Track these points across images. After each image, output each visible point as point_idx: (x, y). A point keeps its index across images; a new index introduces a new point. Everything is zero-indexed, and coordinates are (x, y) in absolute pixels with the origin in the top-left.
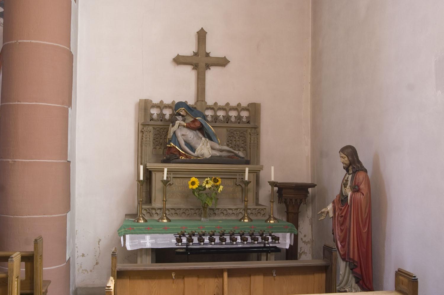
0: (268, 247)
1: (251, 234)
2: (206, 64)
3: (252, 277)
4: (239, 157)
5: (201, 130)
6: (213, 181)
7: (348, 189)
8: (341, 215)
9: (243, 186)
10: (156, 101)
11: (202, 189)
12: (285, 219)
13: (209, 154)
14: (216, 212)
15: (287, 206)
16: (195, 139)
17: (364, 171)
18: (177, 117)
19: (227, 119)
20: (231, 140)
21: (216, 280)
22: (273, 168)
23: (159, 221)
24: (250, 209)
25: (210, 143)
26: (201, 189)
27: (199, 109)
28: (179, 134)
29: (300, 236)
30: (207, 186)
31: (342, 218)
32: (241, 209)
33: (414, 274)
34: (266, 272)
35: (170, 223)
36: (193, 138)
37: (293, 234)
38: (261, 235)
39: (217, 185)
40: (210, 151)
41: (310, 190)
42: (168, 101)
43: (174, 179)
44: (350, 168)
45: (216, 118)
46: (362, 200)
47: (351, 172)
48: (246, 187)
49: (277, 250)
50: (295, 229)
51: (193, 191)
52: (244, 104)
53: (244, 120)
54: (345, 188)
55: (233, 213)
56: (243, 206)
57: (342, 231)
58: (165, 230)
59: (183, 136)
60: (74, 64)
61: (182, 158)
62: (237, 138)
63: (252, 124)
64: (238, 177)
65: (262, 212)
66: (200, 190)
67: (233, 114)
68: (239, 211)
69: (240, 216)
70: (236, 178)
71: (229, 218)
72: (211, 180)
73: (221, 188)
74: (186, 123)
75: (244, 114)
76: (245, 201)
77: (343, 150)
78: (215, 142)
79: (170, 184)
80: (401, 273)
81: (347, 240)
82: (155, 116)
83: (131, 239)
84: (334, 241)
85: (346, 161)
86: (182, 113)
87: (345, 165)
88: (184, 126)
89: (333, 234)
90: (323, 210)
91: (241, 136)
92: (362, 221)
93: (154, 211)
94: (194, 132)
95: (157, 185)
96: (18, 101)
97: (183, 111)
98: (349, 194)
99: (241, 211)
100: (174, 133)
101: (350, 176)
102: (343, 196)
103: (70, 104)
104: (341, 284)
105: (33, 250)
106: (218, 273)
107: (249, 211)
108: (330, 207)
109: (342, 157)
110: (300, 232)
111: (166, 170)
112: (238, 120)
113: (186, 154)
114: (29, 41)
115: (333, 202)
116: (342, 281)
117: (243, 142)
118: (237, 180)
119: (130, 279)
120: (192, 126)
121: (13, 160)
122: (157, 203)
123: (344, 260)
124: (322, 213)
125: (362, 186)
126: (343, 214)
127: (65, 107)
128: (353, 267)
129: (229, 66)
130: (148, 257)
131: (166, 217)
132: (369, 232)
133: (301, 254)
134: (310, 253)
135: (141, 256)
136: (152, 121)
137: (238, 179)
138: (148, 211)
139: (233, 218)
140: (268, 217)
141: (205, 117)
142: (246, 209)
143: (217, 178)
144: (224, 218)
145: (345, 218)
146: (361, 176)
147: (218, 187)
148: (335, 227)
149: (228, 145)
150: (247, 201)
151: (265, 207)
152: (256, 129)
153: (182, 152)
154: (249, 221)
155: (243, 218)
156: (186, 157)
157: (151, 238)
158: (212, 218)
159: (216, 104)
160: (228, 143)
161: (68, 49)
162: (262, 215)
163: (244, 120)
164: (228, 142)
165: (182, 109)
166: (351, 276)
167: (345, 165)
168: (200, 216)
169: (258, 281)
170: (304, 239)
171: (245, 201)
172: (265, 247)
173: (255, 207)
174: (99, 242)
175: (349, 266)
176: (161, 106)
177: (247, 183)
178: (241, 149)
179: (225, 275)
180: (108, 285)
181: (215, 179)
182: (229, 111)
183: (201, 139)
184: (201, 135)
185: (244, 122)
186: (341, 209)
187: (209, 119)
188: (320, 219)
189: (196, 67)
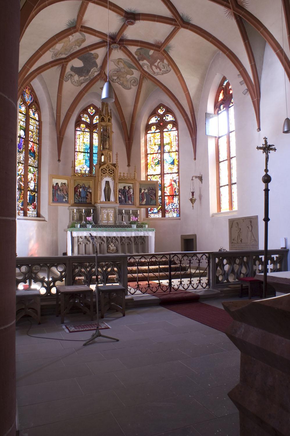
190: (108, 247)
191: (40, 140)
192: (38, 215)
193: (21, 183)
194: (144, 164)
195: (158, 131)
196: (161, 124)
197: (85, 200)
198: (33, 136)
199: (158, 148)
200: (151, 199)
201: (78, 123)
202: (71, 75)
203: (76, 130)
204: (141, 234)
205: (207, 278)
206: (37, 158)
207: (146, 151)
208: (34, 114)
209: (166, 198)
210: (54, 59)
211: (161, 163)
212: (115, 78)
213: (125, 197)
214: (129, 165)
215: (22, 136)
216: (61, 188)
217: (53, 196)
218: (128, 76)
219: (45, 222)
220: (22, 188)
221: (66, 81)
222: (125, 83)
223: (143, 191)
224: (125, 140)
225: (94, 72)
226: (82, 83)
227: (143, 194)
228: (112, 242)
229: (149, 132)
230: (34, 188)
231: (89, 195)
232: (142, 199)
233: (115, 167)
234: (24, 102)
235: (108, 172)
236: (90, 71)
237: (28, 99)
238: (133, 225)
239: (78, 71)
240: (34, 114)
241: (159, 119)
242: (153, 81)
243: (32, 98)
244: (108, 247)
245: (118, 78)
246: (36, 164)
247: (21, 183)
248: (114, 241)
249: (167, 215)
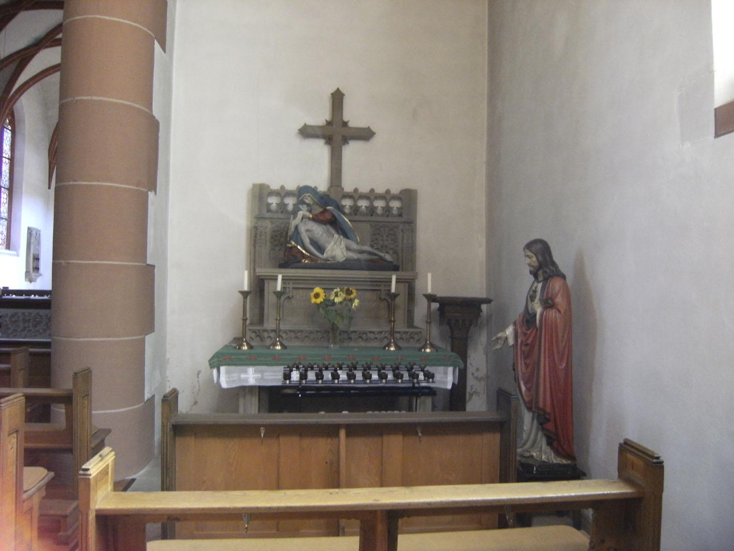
0: (417, 388)
1: (394, 369)
2: (343, 136)
3: (385, 438)
4: (385, 261)
5: (334, 223)
6: (345, 292)
7: (537, 303)
8: (525, 343)
9: (390, 300)
10: (275, 186)
11: (330, 304)
12: (449, 349)
13: (342, 256)
14: (353, 336)
15: (452, 331)
16: (325, 235)
17: (562, 277)
18: (301, 207)
19: (372, 210)
20: (377, 239)
21: (329, 440)
22: (429, 275)
23: (270, 348)
24: (399, 332)
25: (344, 242)
26: (328, 303)
27: (333, 196)
28: (302, 229)
29: (470, 370)
30: (337, 300)
31: (528, 348)
32: (386, 332)
33: (655, 452)
34: (407, 429)
35: (285, 351)
36: (322, 235)
37: (457, 368)
38: (409, 370)
39: (351, 298)
40: (345, 253)
41: (484, 307)
42: (291, 186)
43: (295, 292)
44: (540, 273)
45: (355, 210)
46: (558, 320)
47: (541, 278)
48: (393, 302)
49: (431, 392)
50: (461, 361)
51: (318, 306)
52: (395, 191)
53: (395, 212)
54: (533, 303)
55: (376, 338)
56: (387, 329)
57: (527, 366)
58: (273, 360)
59: (308, 233)
60: (161, 134)
61: (306, 262)
62: (384, 237)
63: (405, 218)
64: (382, 288)
65: (416, 337)
66: (327, 306)
67: (379, 204)
68: (384, 334)
69: (386, 342)
70: (381, 290)
71: (369, 345)
72: (343, 292)
73: (356, 302)
74: (312, 215)
75: (395, 204)
76: (391, 321)
77: (529, 246)
78: (352, 240)
79: (289, 297)
80: (632, 450)
81: (535, 380)
82: (274, 207)
83: (227, 372)
84: (515, 380)
85: (533, 261)
86: (307, 201)
87: (532, 269)
88: (309, 219)
89: (514, 370)
90: (499, 335)
91: (391, 234)
92: (558, 353)
93: (266, 335)
94: (324, 227)
95: (270, 299)
96: (75, 181)
97: (309, 198)
98: (539, 310)
99: (387, 335)
100: (296, 227)
101: (540, 285)
102: (529, 314)
103: (153, 186)
104: (524, 444)
105: (71, 388)
106: (331, 431)
107: (398, 336)
108: (509, 331)
109: (528, 256)
110: (470, 364)
111: (280, 277)
112: (386, 212)
113: (312, 256)
114: (89, 98)
115: (515, 324)
116: (527, 441)
117: (392, 242)
118: (381, 293)
119: (195, 439)
120: (321, 218)
121: (67, 261)
122: (270, 324)
123: (529, 409)
124: (498, 339)
125: (559, 300)
126: (529, 342)
127: (142, 189)
128: (542, 420)
129: (375, 139)
130: (253, 399)
131: (279, 341)
132: (568, 370)
133: (471, 395)
134: (484, 393)
135: (244, 396)
136: (269, 214)
137: (383, 290)
138: (258, 334)
139: (376, 344)
140: (423, 343)
141: (340, 208)
142: (392, 332)
143: (351, 289)
144: (363, 344)
145: (532, 346)
146: (556, 285)
147: (351, 301)
148: (517, 360)
149: (372, 246)
150: (394, 321)
151: (420, 330)
152: (411, 224)
153: (307, 254)
154: (396, 350)
155: (389, 345)
156: (312, 260)
157: (256, 372)
158: (345, 345)
159: (356, 190)
160: (372, 243)
161: (147, 110)
162: (415, 341)
163: (395, 212)
164: (373, 241)
165: (307, 195)
166: (540, 434)
167: (532, 269)
168: (328, 341)
169: (395, 442)
170: (476, 374)
171: (391, 321)
172: (414, 387)
173: (407, 330)
174: (198, 374)
175: (538, 419)
176: (282, 193)
177: (395, 296)
178: (391, 252)
179: (342, 433)
180: (84, 467)
181: (348, 290)
182: (373, 201)
183: (333, 236)
184: (332, 231)
185: (394, 216)
186: (525, 334)
187: (347, 211)
188: (494, 349)
189: (329, 140)
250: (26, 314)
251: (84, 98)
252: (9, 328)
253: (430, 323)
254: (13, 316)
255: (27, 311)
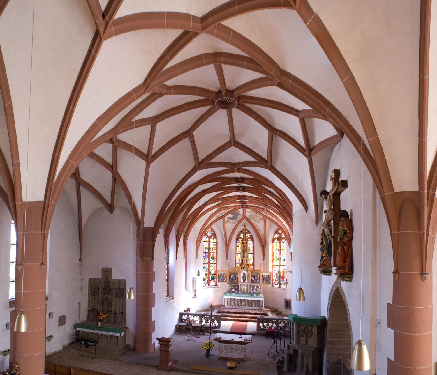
190: (241, 303)
191: (217, 251)
192: (216, 285)
193: (207, 272)
194: (271, 259)
195: (278, 242)
196: (280, 238)
197: (234, 280)
198: (213, 250)
199: (278, 251)
200: (268, 280)
201: (237, 239)
202: (229, 221)
203: (236, 243)
204: (257, 299)
205: (190, 316)
206: (215, 259)
207: (273, 252)
208: (213, 240)
209: (281, 278)
210: (217, 218)
211: (279, 259)
212: (251, 218)
213: (255, 279)
214: (264, 260)
215: (207, 252)
216: (223, 275)
217: (219, 279)
218: (258, 217)
219: (219, 288)
220: (207, 274)
221: (227, 223)
222: (257, 220)
223: (264, 276)
224: (262, 247)
225: (240, 217)
226: (235, 223)
227: (264, 278)
228: (243, 301)
229: (274, 242)
230: (214, 273)
231: (237, 278)
232: (263, 280)
233: (248, 266)
234: (208, 236)
235: (244, 268)
236: (238, 217)
237: (209, 233)
238: (254, 294)
239: (232, 218)
240: (213, 240)
241: (279, 235)
242: (270, 220)
243: (212, 233)
244: (241, 303)
245: (253, 218)
246: (215, 262)
247: (207, 272)
248: (244, 301)
249: (281, 286)
250: (232, 346)
251: (421, 368)
252: (224, 351)
253: (211, 307)
254: (225, 347)
255: (232, 345)
